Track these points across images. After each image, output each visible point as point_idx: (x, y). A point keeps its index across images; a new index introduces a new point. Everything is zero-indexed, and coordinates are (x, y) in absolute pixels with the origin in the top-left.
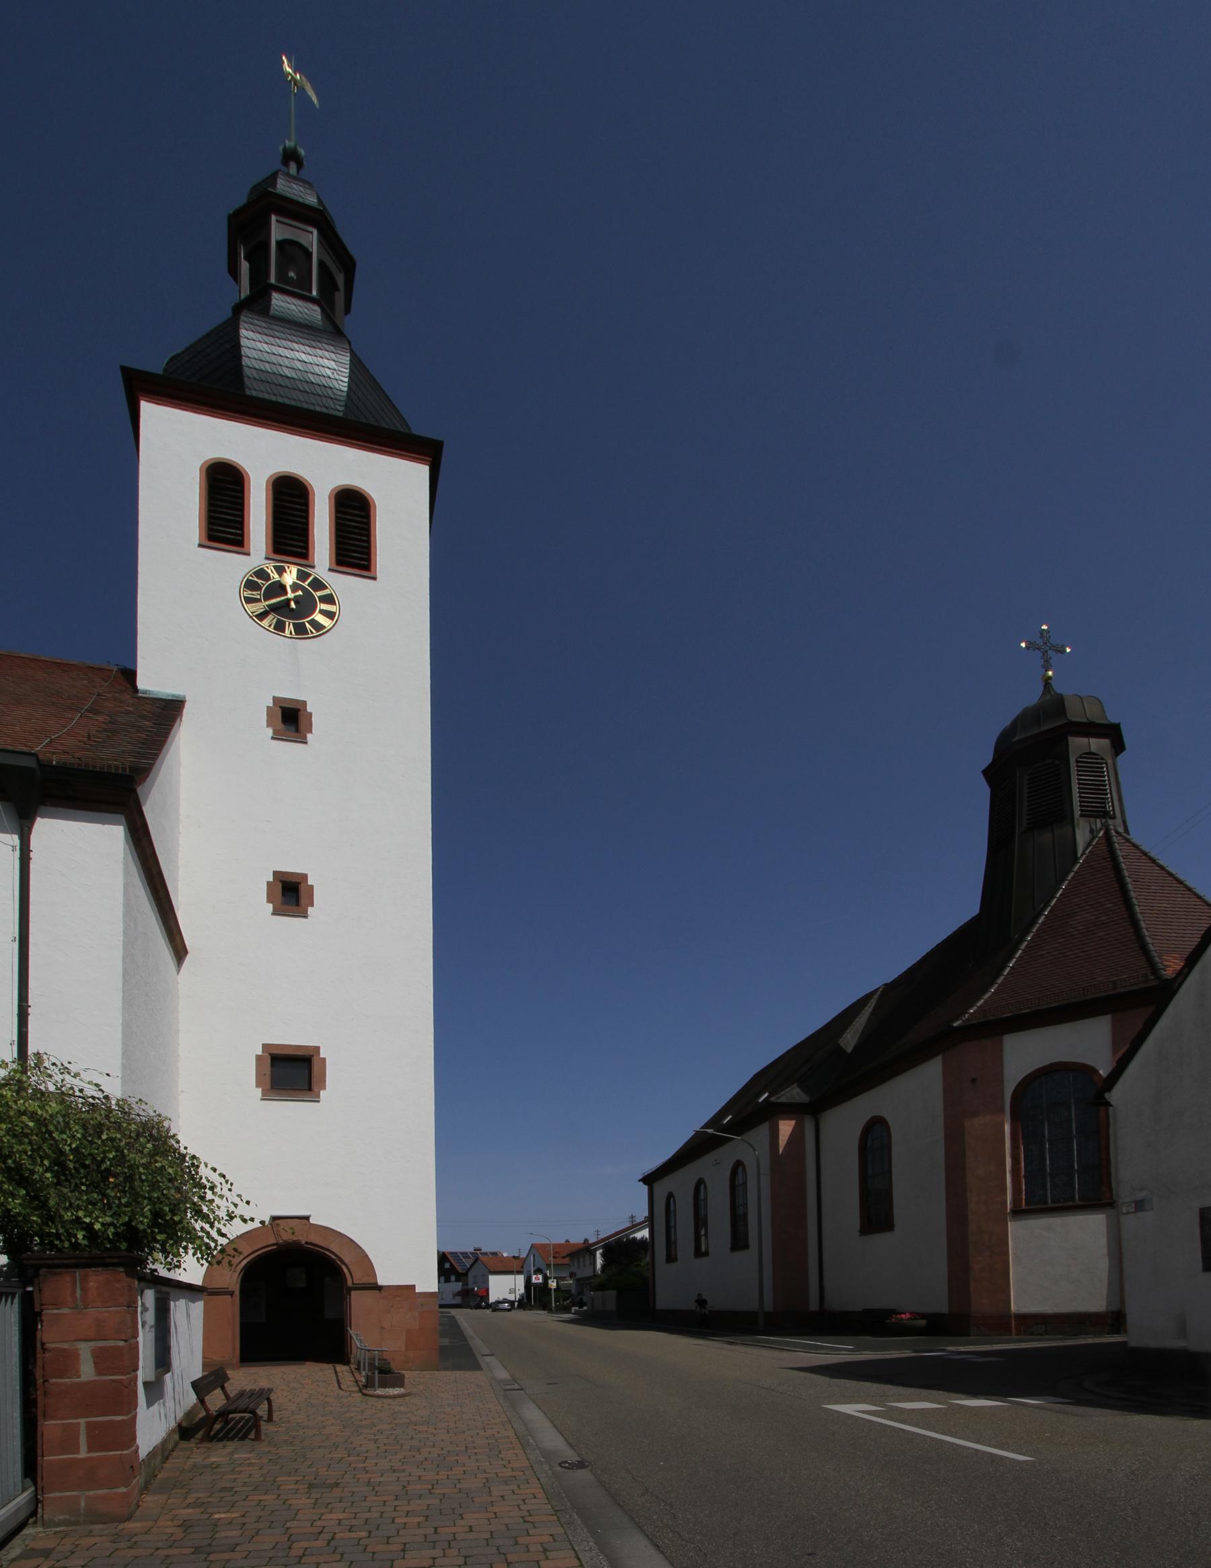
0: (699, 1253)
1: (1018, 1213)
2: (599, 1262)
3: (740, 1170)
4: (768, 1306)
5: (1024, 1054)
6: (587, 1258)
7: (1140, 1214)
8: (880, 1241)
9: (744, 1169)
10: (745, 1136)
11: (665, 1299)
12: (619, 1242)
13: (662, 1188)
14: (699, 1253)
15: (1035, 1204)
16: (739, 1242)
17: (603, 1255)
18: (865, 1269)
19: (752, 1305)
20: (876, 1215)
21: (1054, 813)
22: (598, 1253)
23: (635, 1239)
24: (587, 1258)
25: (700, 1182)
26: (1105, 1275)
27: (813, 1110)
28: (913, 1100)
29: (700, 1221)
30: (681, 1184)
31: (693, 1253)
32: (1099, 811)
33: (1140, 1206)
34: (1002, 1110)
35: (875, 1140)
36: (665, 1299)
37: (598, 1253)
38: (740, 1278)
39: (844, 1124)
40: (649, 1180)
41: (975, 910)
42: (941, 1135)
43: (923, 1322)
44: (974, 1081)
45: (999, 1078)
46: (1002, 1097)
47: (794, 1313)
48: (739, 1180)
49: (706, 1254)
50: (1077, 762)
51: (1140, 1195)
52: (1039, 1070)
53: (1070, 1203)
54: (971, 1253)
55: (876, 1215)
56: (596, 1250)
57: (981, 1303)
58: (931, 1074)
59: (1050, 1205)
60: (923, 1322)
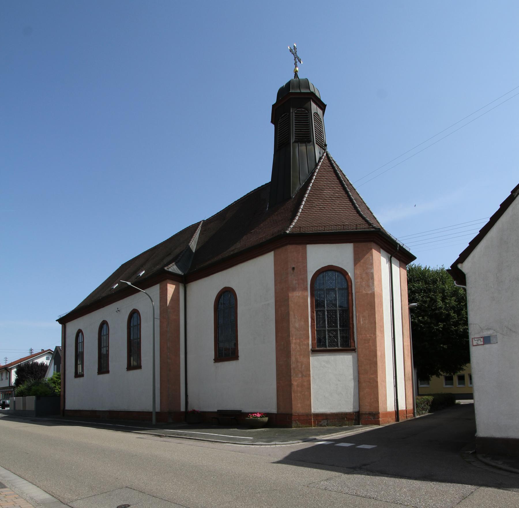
0: (78, 375)
1: (314, 351)
2: (14, 377)
3: (80, 334)
4: (158, 409)
5: (319, 256)
6: (4, 375)
7: (487, 346)
8: (228, 367)
9: (82, 334)
10: (148, 291)
11: (71, 403)
12: (27, 365)
13: (73, 327)
14: (78, 375)
15: (322, 346)
16: (134, 362)
17: (17, 373)
18: (212, 384)
19: (150, 408)
20: (226, 350)
21: (305, 138)
22: (13, 372)
23: (36, 364)
24: (4, 375)
25: (104, 324)
26: (352, 390)
27: (184, 280)
28: (253, 280)
29: (79, 356)
30: (89, 324)
31: (97, 371)
32: (323, 146)
33: (487, 340)
34: (306, 289)
35: (226, 305)
36: (71, 403)
37: (13, 372)
38: (138, 390)
39: (204, 292)
40: (63, 321)
41: (270, 181)
42: (272, 301)
43: (266, 419)
44: (293, 269)
45: (306, 271)
46: (307, 281)
47: (176, 416)
48: (104, 332)
49: (82, 376)
50: (296, 129)
51: (486, 333)
52: (323, 268)
53: (336, 348)
54: (289, 377)
55: (226, 350)
56: (11, 369)
57: (297, 408)
58: (265, 265)
59: (328, 348)
60: (266, 419)
